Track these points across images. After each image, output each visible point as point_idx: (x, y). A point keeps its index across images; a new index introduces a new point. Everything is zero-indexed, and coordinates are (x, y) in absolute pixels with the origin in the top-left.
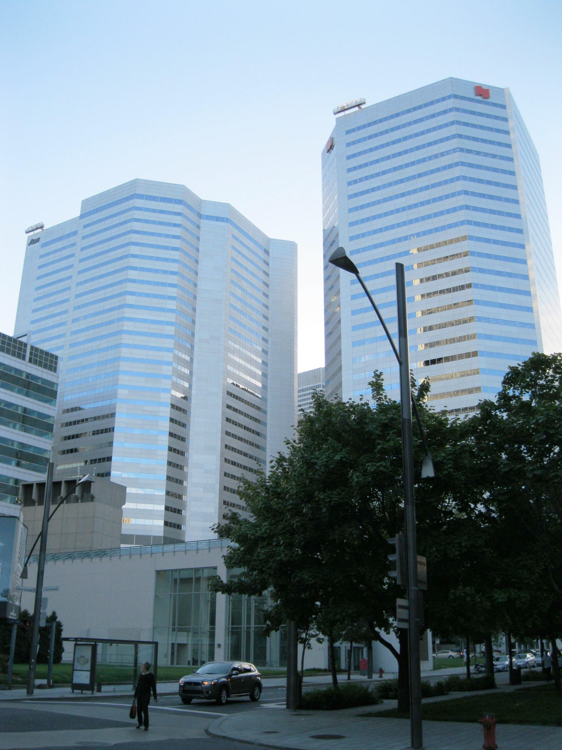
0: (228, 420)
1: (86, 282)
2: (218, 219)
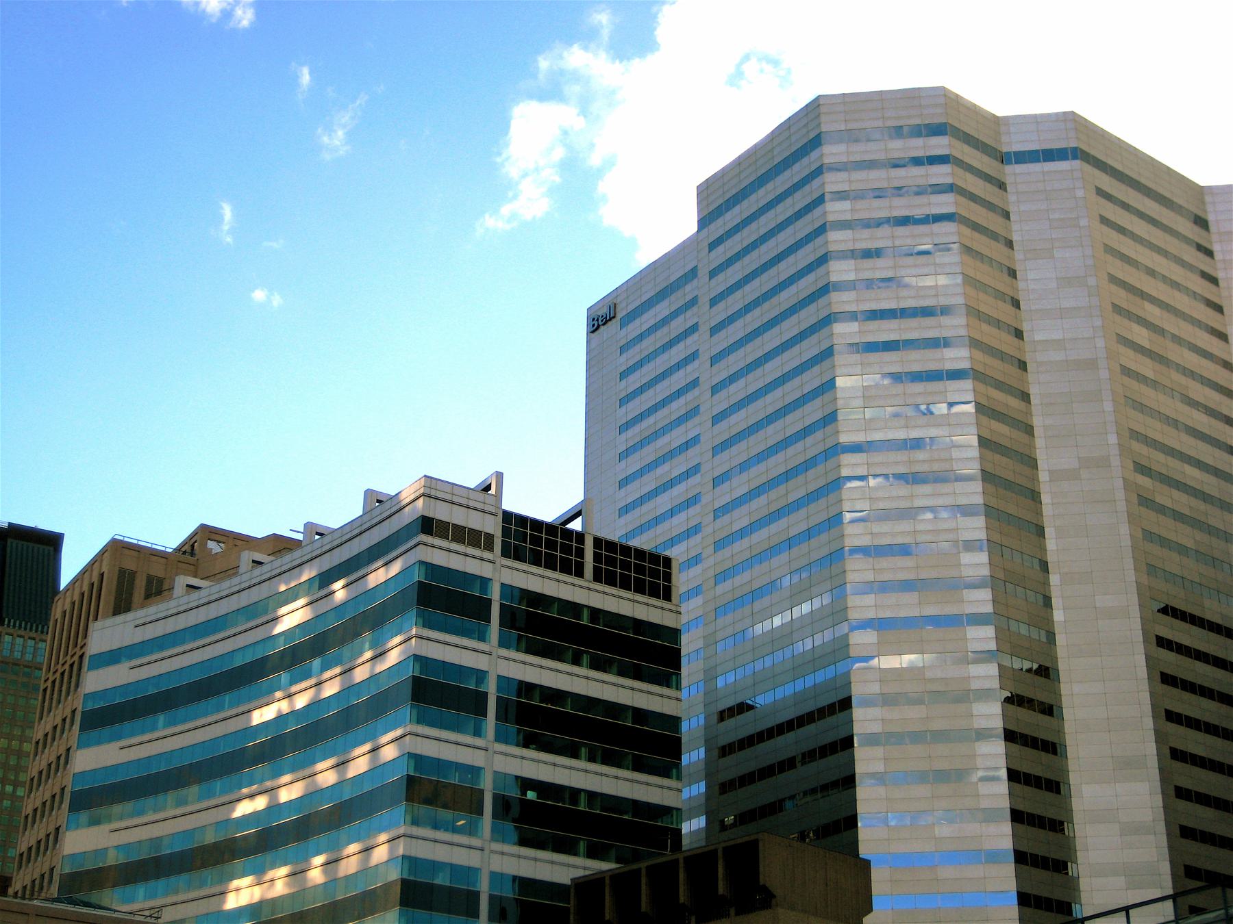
2: (1049, 155)
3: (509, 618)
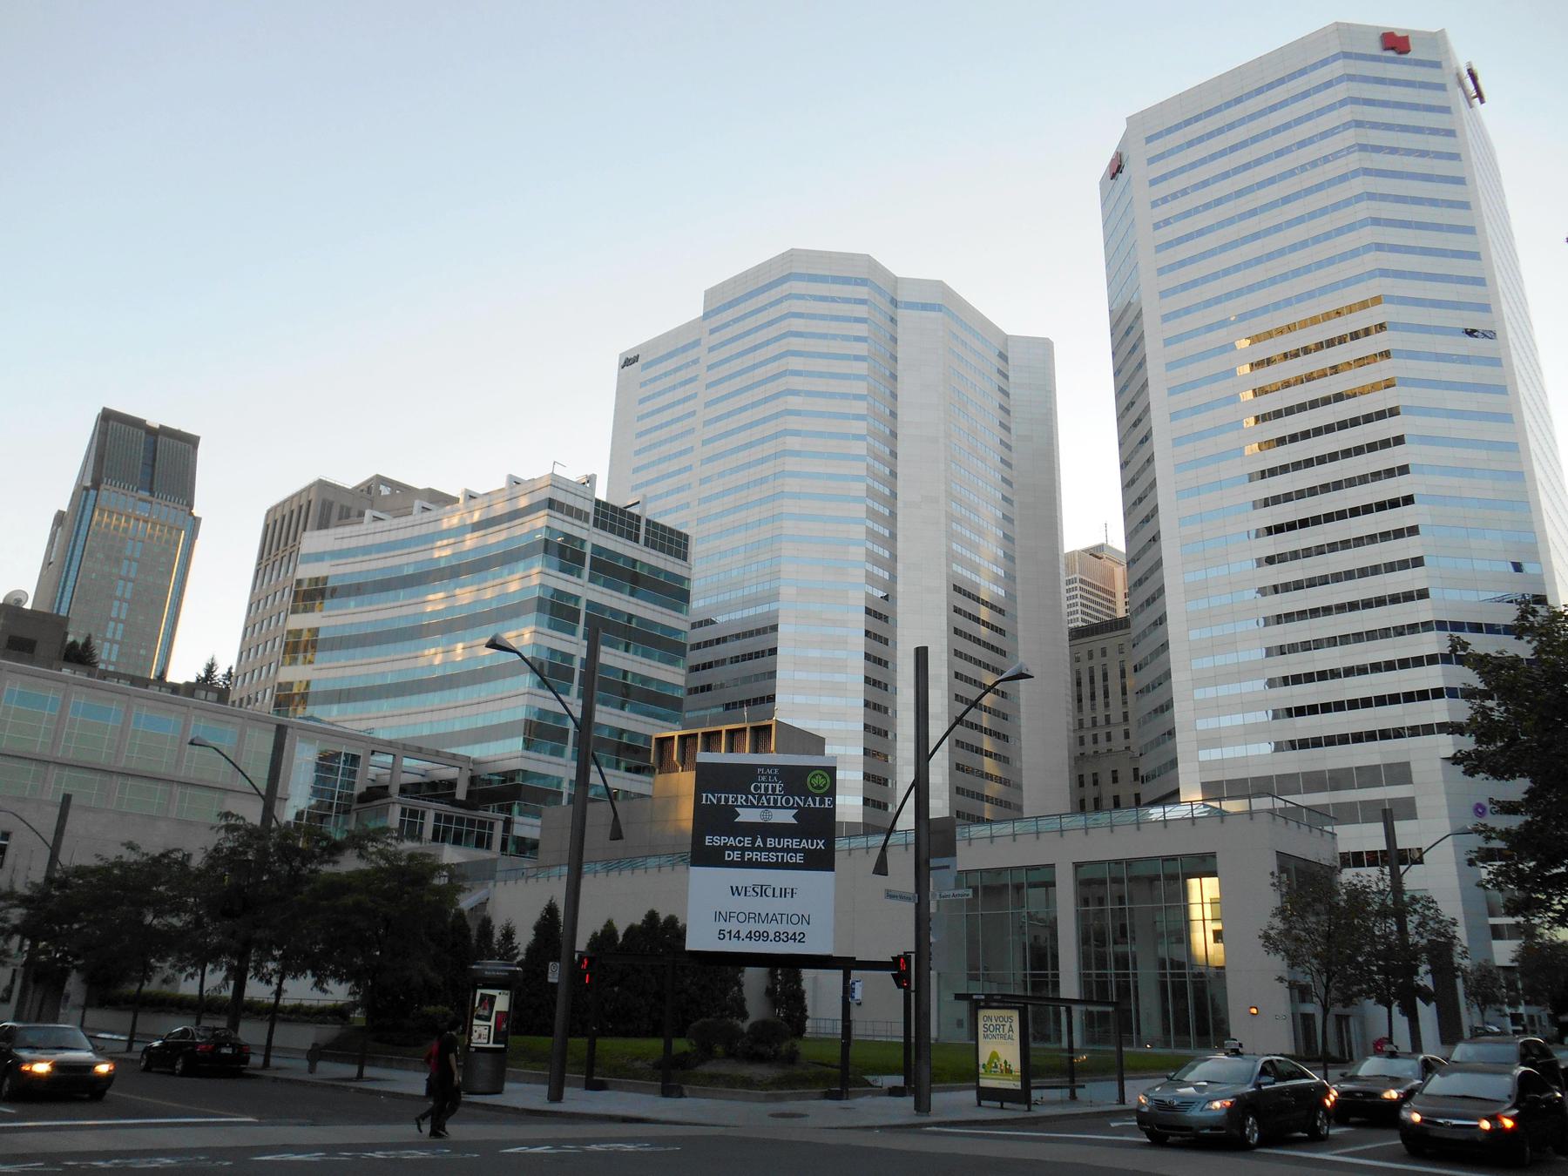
0: (956, 631)
1: (718, 419)
2: (924, 307)
3: (597, 566)
